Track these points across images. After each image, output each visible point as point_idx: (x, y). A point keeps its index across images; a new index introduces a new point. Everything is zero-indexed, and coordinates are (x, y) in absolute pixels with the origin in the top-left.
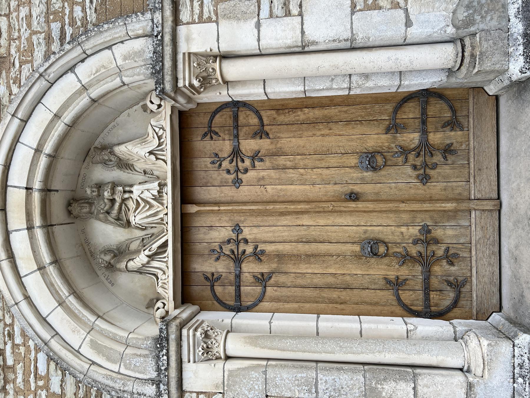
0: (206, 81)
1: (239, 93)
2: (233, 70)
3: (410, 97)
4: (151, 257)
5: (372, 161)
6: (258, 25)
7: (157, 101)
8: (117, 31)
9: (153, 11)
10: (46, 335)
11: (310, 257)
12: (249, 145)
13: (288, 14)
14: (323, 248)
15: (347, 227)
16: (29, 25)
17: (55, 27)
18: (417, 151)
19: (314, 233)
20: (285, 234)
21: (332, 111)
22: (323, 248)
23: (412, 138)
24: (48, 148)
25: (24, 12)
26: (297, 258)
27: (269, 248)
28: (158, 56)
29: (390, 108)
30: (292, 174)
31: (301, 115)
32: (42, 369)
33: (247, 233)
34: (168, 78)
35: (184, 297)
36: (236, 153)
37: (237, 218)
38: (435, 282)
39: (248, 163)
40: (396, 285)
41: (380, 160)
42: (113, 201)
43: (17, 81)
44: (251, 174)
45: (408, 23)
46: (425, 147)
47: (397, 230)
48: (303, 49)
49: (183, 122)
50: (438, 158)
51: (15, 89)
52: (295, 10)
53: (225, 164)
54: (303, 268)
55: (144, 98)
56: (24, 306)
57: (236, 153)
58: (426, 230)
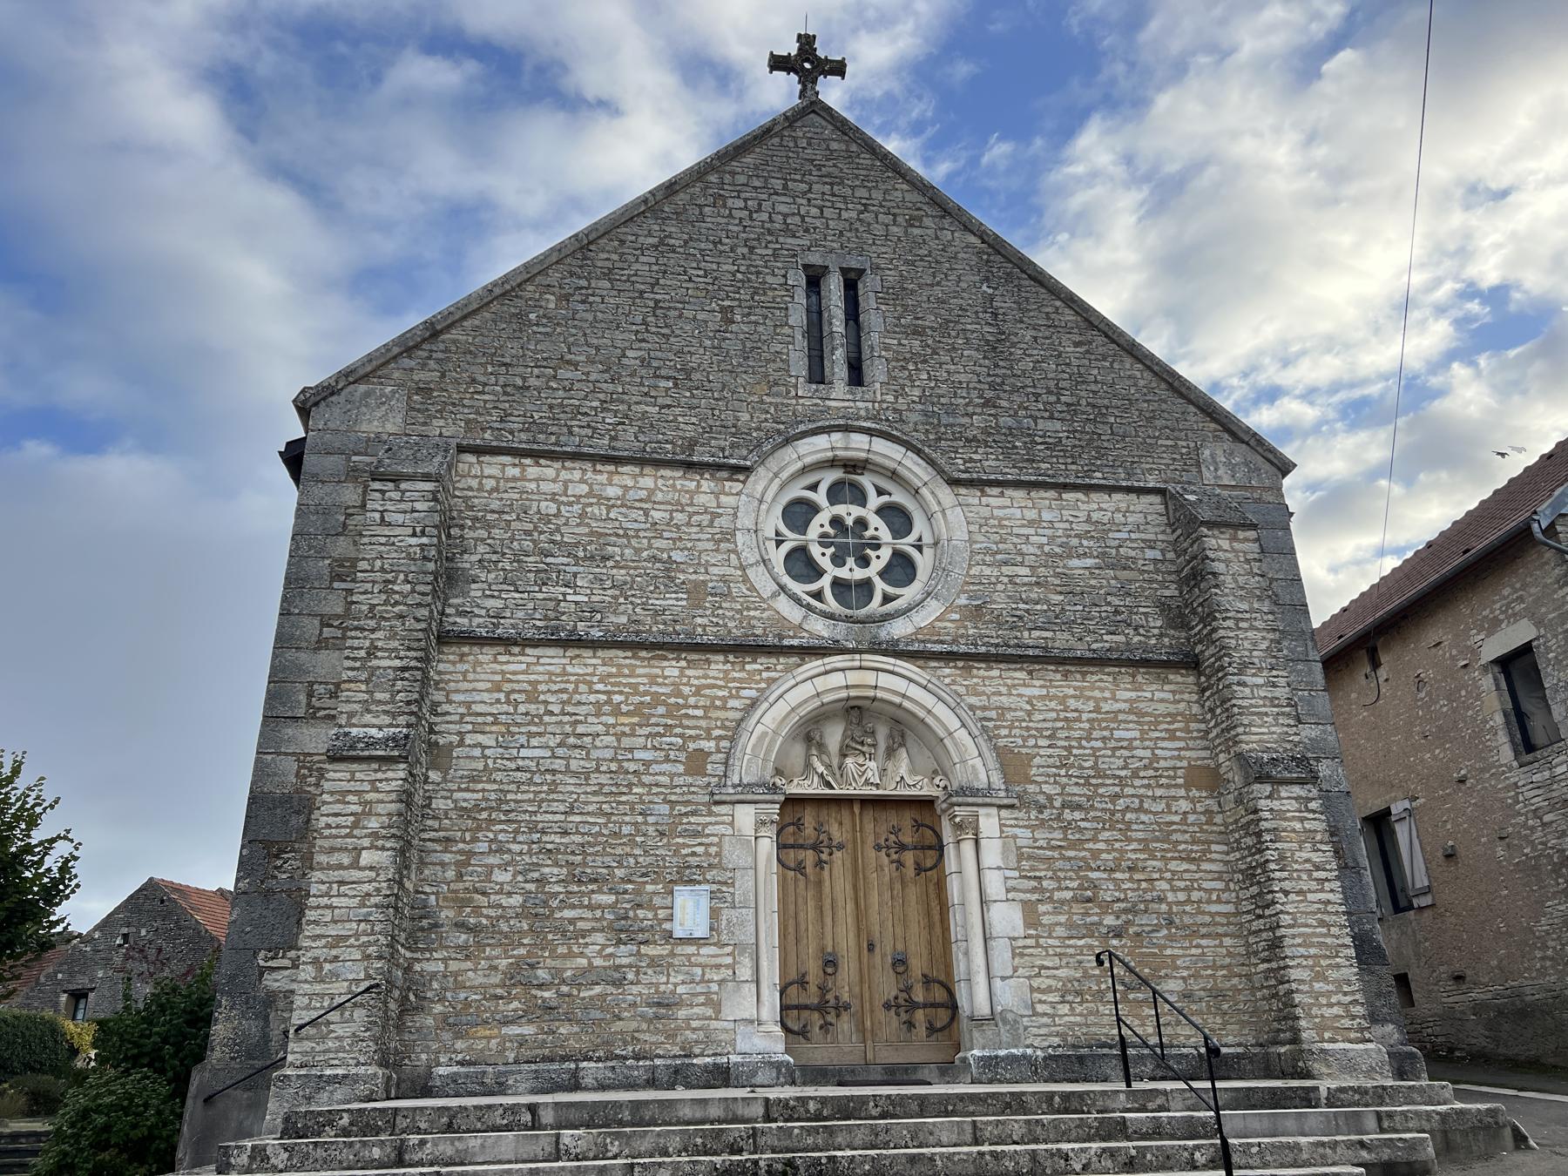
0: (959, 827)
1: (950, 851)
2: (968, 848)
3: (951, 994)
4: (821, 776)
5: (900, 963)
6: (999, 868)
7: (942, 784)
8: (992, 764)
9: (1007, 790)
10: (771, 699)
11: (820, 909)
12: (909, 858)
13: (1008, 891)
14: (828, 920)
15: (845, 941)
16: (994, 694)
17: (993, 714)
18: (910, 1001)
19: (841, 913)
20: (838, 888)
21: (938, 930)
22: (828, 920)
23: (919, 996)
24: (906, 704)
25: (1004, 690)
26: (819, 898)
27: (826, 873)
28: (975, 792)
29: (942, 978)
30: (887, 895)
31: (934, 904)
32: (744, 693)
33: (838, 854)
34: (960, 799)
35: (792, 802)
36: (902, 847)
37: (850, 846)
38: (805, 1014)
39: (895, 857)
40: (802, 982)
41: (900, 969)
42: (862, 743)
43: (954, 682)
44: (886, 860)
45: (1003, 978)
46: (912, 1006)
47: (845, 984)
48: (984, 902)
49: (927, 803)
50: (904, 1017)
51: (947, 681)
52: (1010, 896)
53: (893, 837)
54: (811, 904)
55: (945, 775)
56: (793, 682)
57: (902, 847)
58: (847, 1007)
